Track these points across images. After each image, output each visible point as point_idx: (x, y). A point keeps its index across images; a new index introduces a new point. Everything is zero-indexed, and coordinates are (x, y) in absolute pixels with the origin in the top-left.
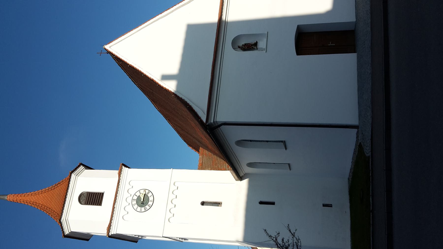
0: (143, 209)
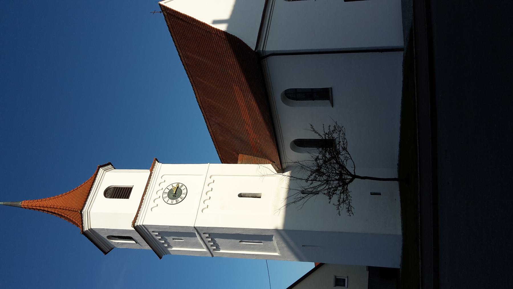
0: (174, 202)
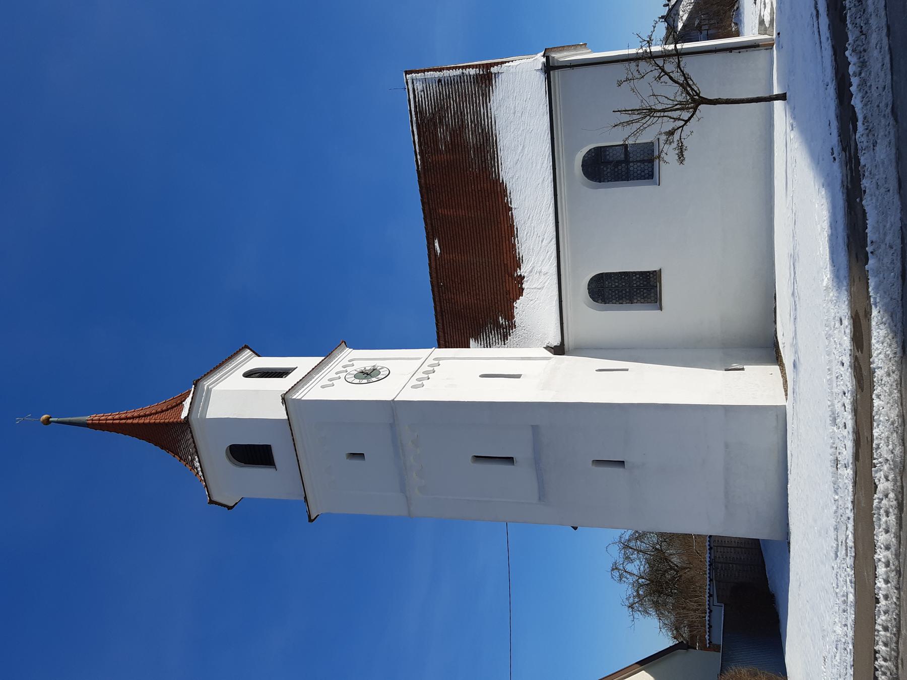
0: (365, 381)
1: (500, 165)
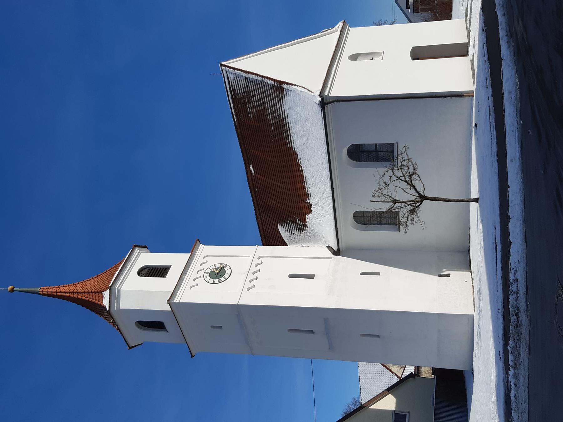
0: (217, 281)
1: (292, 141)
